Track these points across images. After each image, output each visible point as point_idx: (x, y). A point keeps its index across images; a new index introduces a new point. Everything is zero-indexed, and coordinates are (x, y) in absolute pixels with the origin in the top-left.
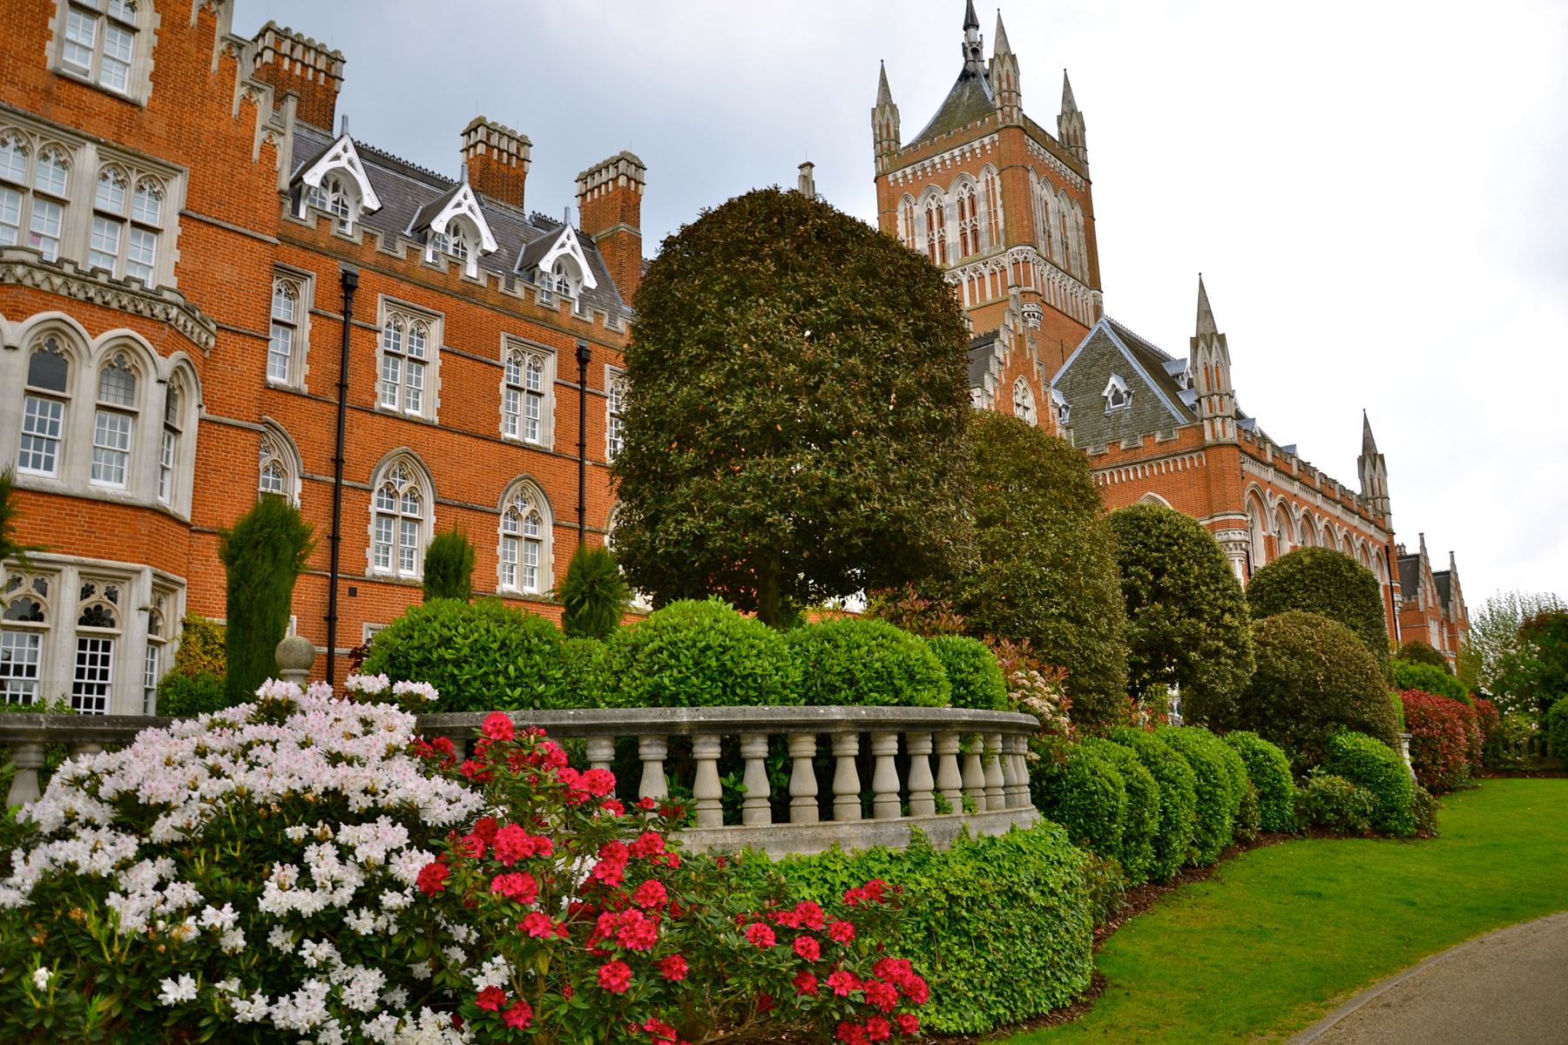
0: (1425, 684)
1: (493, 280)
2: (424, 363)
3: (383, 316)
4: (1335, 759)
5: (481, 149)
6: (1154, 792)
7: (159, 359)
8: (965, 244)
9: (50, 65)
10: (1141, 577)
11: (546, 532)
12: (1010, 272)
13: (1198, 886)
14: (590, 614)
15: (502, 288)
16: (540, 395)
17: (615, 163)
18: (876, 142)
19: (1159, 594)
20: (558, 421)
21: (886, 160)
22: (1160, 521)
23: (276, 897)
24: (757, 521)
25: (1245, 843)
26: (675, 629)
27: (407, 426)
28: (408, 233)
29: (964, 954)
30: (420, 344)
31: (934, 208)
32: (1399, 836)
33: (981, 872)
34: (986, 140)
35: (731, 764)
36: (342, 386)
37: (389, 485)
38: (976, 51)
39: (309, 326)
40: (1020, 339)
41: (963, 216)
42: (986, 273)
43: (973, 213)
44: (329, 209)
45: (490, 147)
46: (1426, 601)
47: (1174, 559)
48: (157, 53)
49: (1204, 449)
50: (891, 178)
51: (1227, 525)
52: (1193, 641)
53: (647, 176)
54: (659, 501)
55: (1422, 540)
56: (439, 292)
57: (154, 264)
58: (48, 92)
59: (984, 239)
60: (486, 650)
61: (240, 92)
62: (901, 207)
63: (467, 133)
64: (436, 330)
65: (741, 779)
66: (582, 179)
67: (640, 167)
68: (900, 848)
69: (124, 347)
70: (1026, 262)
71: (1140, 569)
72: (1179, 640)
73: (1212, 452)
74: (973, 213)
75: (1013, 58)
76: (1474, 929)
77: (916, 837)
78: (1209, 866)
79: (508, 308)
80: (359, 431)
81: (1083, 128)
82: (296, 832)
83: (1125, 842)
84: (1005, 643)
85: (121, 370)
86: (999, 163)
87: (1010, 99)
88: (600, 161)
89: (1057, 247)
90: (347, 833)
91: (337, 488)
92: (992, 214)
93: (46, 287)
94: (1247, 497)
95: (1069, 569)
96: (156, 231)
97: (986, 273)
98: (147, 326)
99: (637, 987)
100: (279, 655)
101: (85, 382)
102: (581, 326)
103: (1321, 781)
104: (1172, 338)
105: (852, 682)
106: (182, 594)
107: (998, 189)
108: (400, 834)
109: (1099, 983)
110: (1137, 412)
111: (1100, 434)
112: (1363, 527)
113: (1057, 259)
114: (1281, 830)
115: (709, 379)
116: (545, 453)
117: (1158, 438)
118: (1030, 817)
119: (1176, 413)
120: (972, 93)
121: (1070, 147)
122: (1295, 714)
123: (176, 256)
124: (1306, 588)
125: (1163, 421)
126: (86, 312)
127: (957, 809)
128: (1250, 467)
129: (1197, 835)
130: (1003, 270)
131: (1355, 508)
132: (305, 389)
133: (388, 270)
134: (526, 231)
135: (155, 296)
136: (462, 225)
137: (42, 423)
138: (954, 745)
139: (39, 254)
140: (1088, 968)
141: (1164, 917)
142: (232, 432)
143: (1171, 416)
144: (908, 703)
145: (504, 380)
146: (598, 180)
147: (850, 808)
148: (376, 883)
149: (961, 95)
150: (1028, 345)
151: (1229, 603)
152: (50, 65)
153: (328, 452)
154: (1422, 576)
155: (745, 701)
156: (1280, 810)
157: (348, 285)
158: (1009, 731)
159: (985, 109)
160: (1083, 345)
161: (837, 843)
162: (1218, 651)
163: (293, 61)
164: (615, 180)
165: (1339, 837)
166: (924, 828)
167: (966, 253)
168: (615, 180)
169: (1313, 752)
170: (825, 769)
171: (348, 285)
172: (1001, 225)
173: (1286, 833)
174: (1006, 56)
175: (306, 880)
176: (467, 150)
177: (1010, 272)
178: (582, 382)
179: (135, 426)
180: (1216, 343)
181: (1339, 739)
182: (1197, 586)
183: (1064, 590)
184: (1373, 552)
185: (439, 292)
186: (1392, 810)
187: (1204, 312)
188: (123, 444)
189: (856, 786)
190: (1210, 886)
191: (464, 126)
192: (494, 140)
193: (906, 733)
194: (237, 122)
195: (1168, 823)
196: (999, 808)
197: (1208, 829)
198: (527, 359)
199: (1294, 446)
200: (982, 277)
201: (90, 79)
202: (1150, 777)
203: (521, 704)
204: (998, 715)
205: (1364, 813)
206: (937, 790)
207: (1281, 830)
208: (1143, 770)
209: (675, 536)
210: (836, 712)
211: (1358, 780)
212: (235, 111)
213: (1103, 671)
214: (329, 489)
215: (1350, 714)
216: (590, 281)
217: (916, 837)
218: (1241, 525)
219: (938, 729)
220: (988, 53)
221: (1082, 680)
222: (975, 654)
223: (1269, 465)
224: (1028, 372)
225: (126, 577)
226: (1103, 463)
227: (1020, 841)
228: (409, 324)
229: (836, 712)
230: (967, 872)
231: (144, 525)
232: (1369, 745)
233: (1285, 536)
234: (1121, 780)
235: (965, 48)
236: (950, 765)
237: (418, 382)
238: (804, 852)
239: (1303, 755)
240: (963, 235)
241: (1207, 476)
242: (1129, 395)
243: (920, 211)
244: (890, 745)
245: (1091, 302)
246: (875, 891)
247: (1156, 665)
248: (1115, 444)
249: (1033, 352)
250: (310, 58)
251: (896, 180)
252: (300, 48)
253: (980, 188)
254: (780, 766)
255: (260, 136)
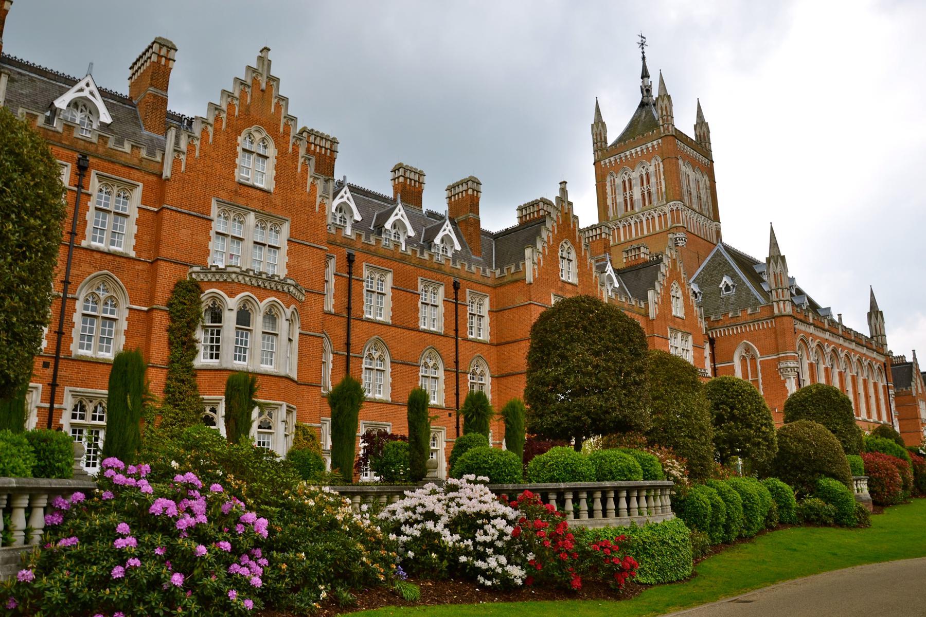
0: (884, 449)
1: (414, 252)
2: (384, 294)
3: (366, 273)
4: (819, 490)
5: (401, 179)
6: (723, 507)
7: (286, 310)
8: (644, 199)
9: (236, 180)
10: (724, 410)
11: (441, 374)
12: (669, 215)
13: (744, 545)
14: (476, 422)
15: (418, 255)
16: (437, 306)
17: (466, 182)
18: (594, 143)
19: (733, 417)
20: (445, 319)
21: (600, 153)
22: (734, 384)
23: (480, 538)
24: (578, 418)
25: (772, 529)
26: (557, 458)
27: (377, 326)
28: (372, 228)
29: (648, 560)
30: (382, 285)
31: (626, 179)
32: (849, 527)
33: (653, 534)
34: (655, 143)
35: (576, 500)
36: (349, 309)
37: (370, 355)
38: (648, 91)
39: (334, 281)
40: (674, 262)
41: (642, 184)
42: (656, 216)
43: (648, 182)
44: (338, 222)
45: (405, 178)
46: (917, 390)
47: (739, 402)
48: (277, 167)
49: (774, 318)
50: (602, 163)
51: (786, 358)
52: (748, 439)
53: (482, 188)
54: (544, 409)
55: (914, 354)
56: (390, 260)
57: (277, 265)
58: (236, 191)
59: (654, 197)
60: (498, 464)
61: (310, 180)
62: (608, 179)
63: (394, 171)
64: (389, 278)
65: (579, 505)
66: (449, 189)
67: (479, 184)
68: (628, 526)
69: (272, 306)
70: (677, 210)
71: (724, 407)
72: (741, 438)
73: (778, 319)
74: (648, 182)
75: (669, 97)
76: (854, 564)
77: (632, 523)
78: (751, 537)
79: (421, 264)
80: (356, 327)
81: (709, 132)
82: (479, 522)
83: (711, 526)
84: (663, 448)
85: (271, 317)
86: (662, 155)
87: (667, 120)
88: (458, 180)
89: (695, 200)
90: (492, 522)
91: (348, 357)
92: (658, 183)
93: (243, 282)
94: (798, 342)
95: (688, 417)
96: (278, 248)
97: (656, 216)
98: (281, 295)
99: (568, 559)
100: (427, 465)
101: (258, 323)
102: (455, 271)
103: (809, 501)
104: (760, 253)
105: (611, 473)
106: (295, 413)
107: (662, 170)
108: (504, 522)
109: (694, 574)
110: (738, 296)
111: (718, 308)
112: (869, 353)
113: (695, 206)
114: (790, 523)
115: (561, 370)
116: (440, 335)
117: (749, 311)
118: (671, 516)
119: (759, 297)
120: (646, 115)
121: (702, 143)
122: (799, 468)
123: (286, 259)
124: (814, 405)
125: (752, 302)
126: (258, 291)
127: (645, 513)
128: (800, 327)
129: (745, 524)
130: (665, 214)
131: (864, 343)
132: (333, 311)
133: (368, 251)
134: (425, 220)
135: (283, 282)
136: (398, 224)
137: (242, 341)
138: (644, 493)
139: (240, 268)
140: (691, 569)
141: (727, 556)
142: (312, 338)
143: (756, 299)
144: (629, 480)
145: (420, 301)
146: (457, 190)
147: (612, 514)
148: (502, 534)
149: (640, 116)
150: (678, 264)
151: (765, 422)
152: (236, 180)
153: (344, 340)
154: (914, 375)
155: (579, 480)
156: (789, 514)
157: (350, 259)
158: (663, 488)
159: (653, 124)
160: (709, 258)
161: (608, 525)
162: (759, 443)
163: (316, 145)
164: (466, 191)
165: (818, 526)
166: (635, 520)
167: (644, 204)
168: (466, 191)
169: (807, 487)
170: (604, 501)
171: (350, 259)
172: (664, 189)
173: (792, 524)
174: (665, 96)
175: (486, 533)
176: (394, 179)
177: (669, 215)
178: (456, 299)
179: (277, 340)
180: (780, 261)
181: (821, 481)
182: (750, 414)
183: (687, 426)
184: (876, 367)
185: (390, 260)
186: (845, 514)
187: (774, 244)
188: (272, 348)
189: (613, 507)
190: (749, 545)
191: (392, 168)
192: (408, 175)
193: (629, 490)
194: (309, 195)
195: (729, 518)
196: (660, 515)
197: (751, 522)
198: (431, 289)
199: (829, 308)
200: (653, 218)
201: (250, 183)
202: (721, 501)
203: (510, 481)
204: (659, 482)
205: (830, 516)
206: (639, 508)
207: (790, 523)
208: (719, 498)
209: (550, 422)
210: (607, 484)
211: (828, 500)
212: (308, 190)
213: (703, 458)
214: (344, 358)
215: (826, 469)
216: (458, 247)
217: (632, 523)
218: (794, 359)
219: (639, 489)
220: (655, 93)
221: (694, 462)
222: (651, 460)
223: (811, 324)
224: (678, 279)
225: (277, 407)
226: (720, 325)
227: (666, 524)
228: (377, 276)
229: (607, 484)
230: (649, 534)
231: (283, 384)
232: (835, 484)
233: (821, 362)
234: (709, 502)
235: (642, 89)
236: (643, 500)
237: (381, 304)
238: (598, 527)
239: (804, 488)
240: (643, 195)
241: (775, 332)
242: (734, 286)
243: (618, 181)
244: (624, 494)
245: (714, 229)
246: (623, 538)
247: (732, 447)
248: (726, 315)
249: (680, 268)
250: (323, 143)
251: (605, 164)
252: (318, 139)
253: (652, 169)
254: (591, 501)
255: (319, 200)
